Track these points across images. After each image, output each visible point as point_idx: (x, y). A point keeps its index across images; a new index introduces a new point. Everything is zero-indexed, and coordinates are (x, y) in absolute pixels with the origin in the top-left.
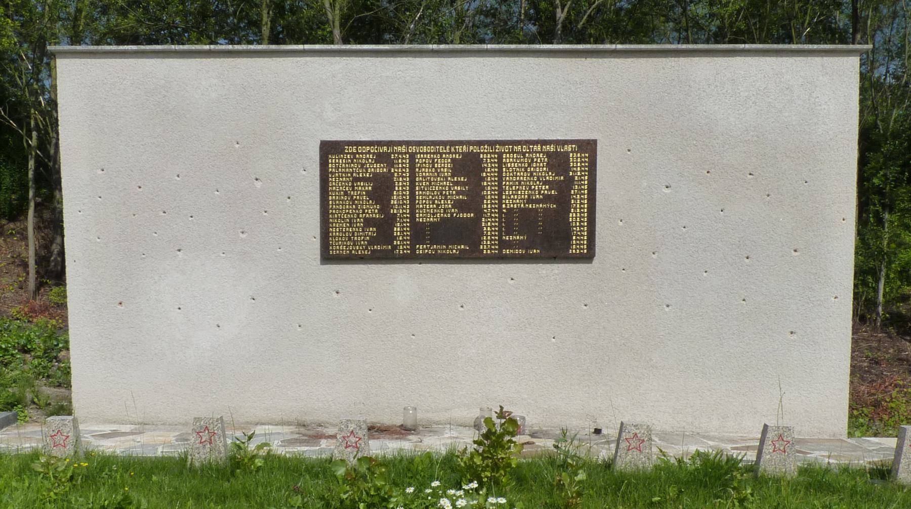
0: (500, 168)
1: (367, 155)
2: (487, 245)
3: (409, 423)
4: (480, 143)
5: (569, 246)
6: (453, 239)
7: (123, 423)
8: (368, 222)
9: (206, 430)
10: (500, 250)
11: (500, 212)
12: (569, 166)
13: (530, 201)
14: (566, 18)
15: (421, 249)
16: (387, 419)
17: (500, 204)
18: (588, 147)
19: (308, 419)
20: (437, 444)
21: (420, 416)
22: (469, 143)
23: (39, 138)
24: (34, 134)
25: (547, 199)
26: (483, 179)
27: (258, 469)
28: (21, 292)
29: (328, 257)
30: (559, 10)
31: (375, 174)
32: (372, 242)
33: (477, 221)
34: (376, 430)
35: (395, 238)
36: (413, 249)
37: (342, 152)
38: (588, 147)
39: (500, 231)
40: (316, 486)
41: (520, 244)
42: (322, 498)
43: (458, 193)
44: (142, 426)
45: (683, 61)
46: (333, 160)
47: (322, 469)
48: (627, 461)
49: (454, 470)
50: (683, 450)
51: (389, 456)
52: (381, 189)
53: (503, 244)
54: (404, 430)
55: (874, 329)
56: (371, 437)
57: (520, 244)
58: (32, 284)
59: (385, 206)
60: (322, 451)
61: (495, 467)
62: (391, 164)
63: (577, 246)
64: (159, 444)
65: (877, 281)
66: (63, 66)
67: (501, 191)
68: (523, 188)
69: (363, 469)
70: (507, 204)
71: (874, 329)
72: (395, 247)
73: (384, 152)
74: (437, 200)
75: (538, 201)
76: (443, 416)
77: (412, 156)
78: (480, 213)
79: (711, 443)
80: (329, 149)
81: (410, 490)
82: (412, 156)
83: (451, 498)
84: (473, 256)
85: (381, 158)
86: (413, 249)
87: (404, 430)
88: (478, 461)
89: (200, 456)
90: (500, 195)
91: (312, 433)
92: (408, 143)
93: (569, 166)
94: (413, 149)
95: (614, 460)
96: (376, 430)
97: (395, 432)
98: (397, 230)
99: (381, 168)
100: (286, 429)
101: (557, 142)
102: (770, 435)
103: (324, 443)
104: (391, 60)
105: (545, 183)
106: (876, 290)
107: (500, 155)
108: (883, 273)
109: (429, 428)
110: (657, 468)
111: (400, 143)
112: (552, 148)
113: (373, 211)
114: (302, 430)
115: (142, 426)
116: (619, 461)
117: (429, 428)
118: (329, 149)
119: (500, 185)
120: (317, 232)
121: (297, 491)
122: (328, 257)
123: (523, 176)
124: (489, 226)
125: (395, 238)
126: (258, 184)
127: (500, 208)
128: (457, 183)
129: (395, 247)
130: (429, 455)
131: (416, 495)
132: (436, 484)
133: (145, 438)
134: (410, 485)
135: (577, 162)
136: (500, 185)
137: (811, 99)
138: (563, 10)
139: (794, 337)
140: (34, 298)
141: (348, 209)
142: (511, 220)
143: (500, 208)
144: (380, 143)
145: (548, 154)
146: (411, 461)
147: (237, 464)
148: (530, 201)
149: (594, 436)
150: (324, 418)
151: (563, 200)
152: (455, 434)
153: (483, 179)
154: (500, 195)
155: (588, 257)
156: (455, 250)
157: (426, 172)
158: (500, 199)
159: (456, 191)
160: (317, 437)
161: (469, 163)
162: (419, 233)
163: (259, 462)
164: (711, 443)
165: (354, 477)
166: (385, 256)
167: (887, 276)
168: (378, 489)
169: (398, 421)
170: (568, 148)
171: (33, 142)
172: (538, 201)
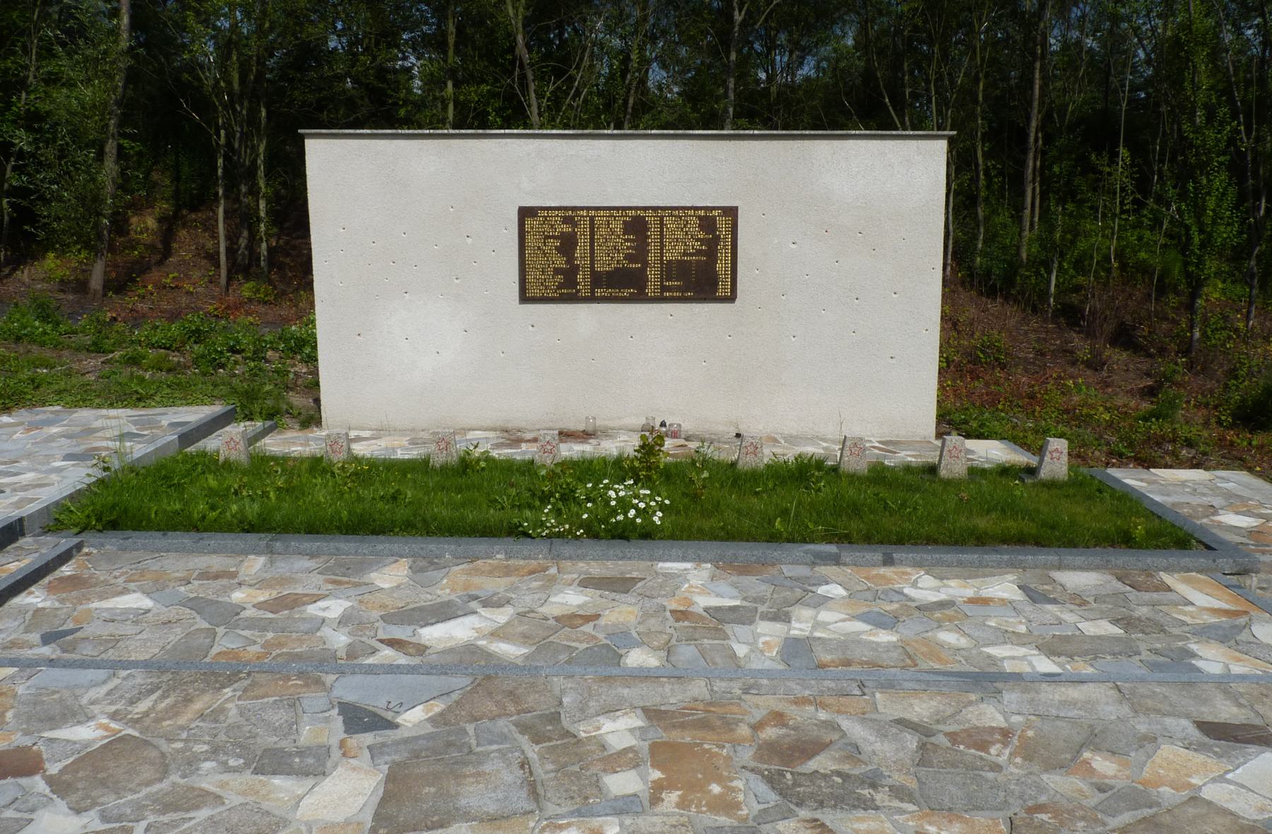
0: (662, 229)
1: (556, 218)
2: (649, 291)
3: (590, 429)
4: (645, 209)
5: (716, 290)
6: (624, 284)
7: (362, 429)
8: (557, 271)
9: (444, 441)
10: (662, 293)
11: (662, 263)
12: (717, 227)
13: (685, 254)
14: (744, 20)
15: (598, 293)
16: (572, 425)
17: (662, 256)
18: (731, 212)
19: (510, 426)
20: (609, 448)
21: (598, 423)
22: (636, 208)
23: (227, 136)
24: (222, 132)
25: (699, 252)
26: (648, 237)
27: (483, 469)
28: (210, 286)
29: (525, 298)
30: (736, 13)
31: (562, 233)
32: (560, 286)
33: (643, 269)
34: (566, 435)
35: (578, 284)
36: (593, 292)
37: (536, 215)
38: (731, 212)
39: (662, 278)
40: (524, 481)
41: (678, 289)
42: (530, 490)
43: (628, 248)
44: (379, 432)
45: (807, 143)
46: (528, 222)
47: (528, 467)
48: (748, 463)
49: (619, 469)
50: (789, 453)
51: (575, 458)
52: (567, 245)
53: (664, 289)
54: (585, 436)
55: (1045, 321)
56: (561, 441)
57: (678, 289)
58: (223, 280)
59: (570, 256)
60: (525, 453)
61: (649, 469)
62: (575, 225)
63: (723, 289)
64: (404, 452)
65: (1050, 273)
66: (309, 144)
67: (662, 246)
68: (678, 245)
69: (558, 470)
70: (668, 256)
71: (1045, 321)
72: (578, 291)
73: (570, 215)
74: (610, 253)
75: (691, 255)
76: (616, 424)
77: (592, 219)
78: (645, 264)
79: (825, 445)
80: (526, 213)
81: (590, 485)
82: (592, 219)
83: (615, 491)
84: (640, 297)
85: (567, 220)
86: (593, 292)
87: (585, 436)
88: (636, 464)
89: (438, 459)
90: (662, 249)
91: (513, 437)
92: (588, 209)
93: (717, 227)
94: (593, 213)
95: (737, 461)
96: (566, 435)
97: (578, 437)
98: (580, 277)
99: (567, 229)
100: (491, 434)
101: (706, 208)
102: (848, 443)
103: (524, 446)
104: (574, 142)
105: (697, 240)
106: (1049, 282)
107: (662, 218)
108: (1056, 265)
109: (606, 433)
110: (768, 466)
111: (582, 208)
112: (702, 213)
113: (561, 262)
114: (506, 435)
115: (379, 432)
116: (740, 463)
117: (606, 433)
118: (526, 213)
119: (661, 242)
120: (516, 278)
121: (512, 485)
122: (525, 298)
123: (680, 235)
124: (652, 274)
125: (578, 284)
126: (469, 241)
127: (662, 260)
128: (627, 240)
129: (578, 291)
130: (604, 459)
131: (594, 488)
132: (606, 481)
133: (383, 443)
134: (590, 481)
135: (722, 225)
136: (661, 242)
137: (899, 182)
138: (740, 12)
139: (893, 361)
140: (227, 294)
141: (542, 261)
142: (669, 270)
143: (662, 260)
144: (566, 209)
145: (700, 217)
146: (591, 462)
147: (466, 465)
148: (685, 254)
149: (735, 440)
150: (523, 424)
151: (711, 254)
152: (626, 438)
153: (648, 237)
154: (662, 249)
155: (731, 298)
156: (625, 293)
157: (603, 231)
158: (662, 253)
159: (626, 245)
160: (517, 442)
161: (637, 223)
162: (598, 279)
163: (483, 464)
164: (825, 445)
165: (552, 476)
166: (571, 297)
167: (1060, 267)
168: (568, 484)
169: (581, 427)
170: (715, 213)
171: (223, 141)
172: (691, 255)
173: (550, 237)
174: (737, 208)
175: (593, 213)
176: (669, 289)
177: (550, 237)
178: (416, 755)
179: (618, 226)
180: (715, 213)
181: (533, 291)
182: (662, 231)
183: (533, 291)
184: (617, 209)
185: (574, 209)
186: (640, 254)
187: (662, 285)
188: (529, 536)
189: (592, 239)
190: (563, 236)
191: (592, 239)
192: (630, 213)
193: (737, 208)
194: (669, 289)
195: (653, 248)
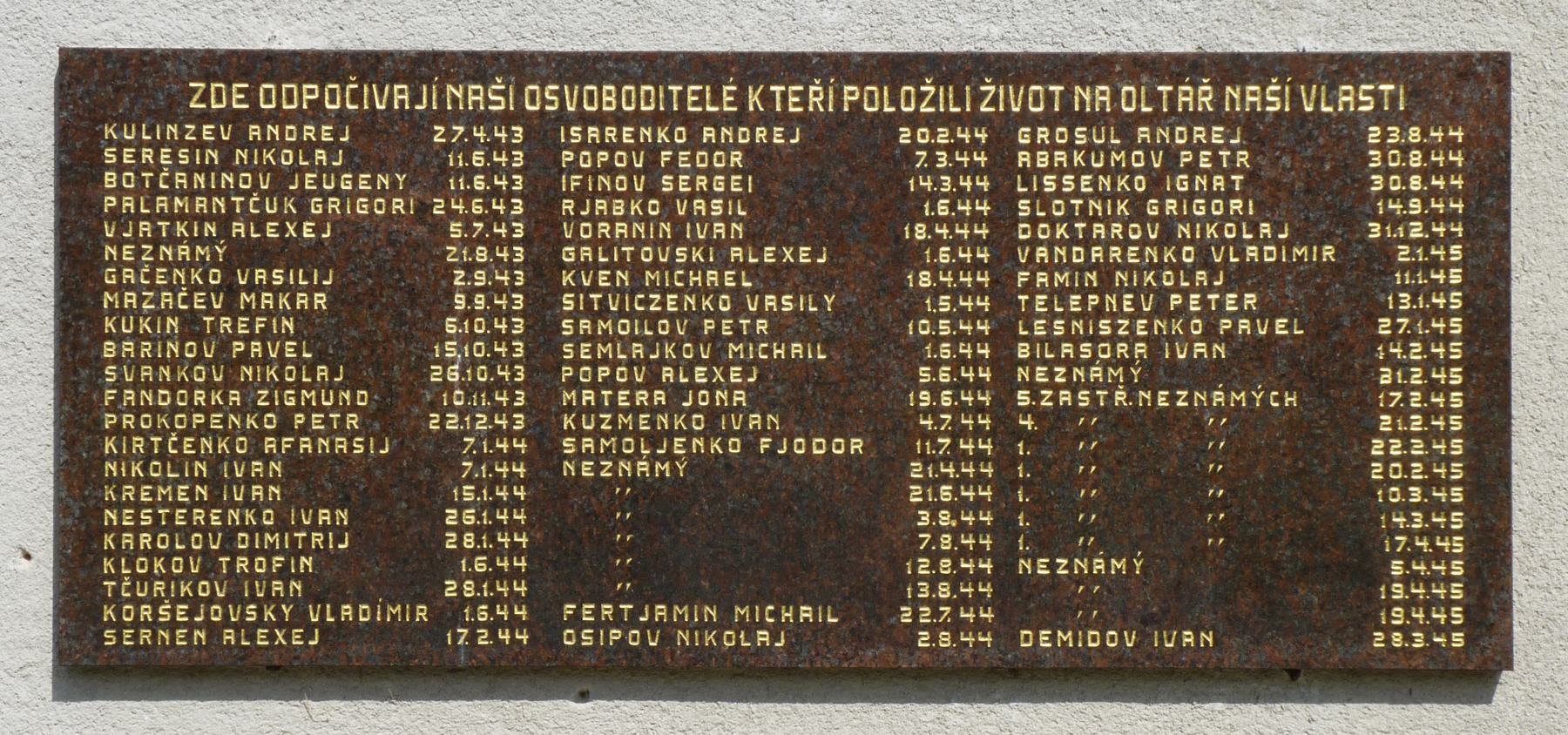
0: (1003, 199)
2: (930, 610)
4: (895, 69)
5: (1368, 615)
8: (308, 479)
10: (1006, 630)
15: (587, 624)
17: (1005, 383)
22: (839, 67)
25: (1249, 359)
31: (348, 227)
33: (880, 478)
35: (449, 563)
36: (546, 623)
37: (173, 110)
38: (1466, 94)
39: (1004, 528)
41: (1113, 604)
43: (781, 329)
46: (124, 149)
52: (380, 304)
53: (1018, 600)
57: (1113, 604)
59: (398, 394)
62: (432, 173)
63: (1416, 603)
68: (1123, 311)
70: (1044, 386)
72: (448, 615)
73: (394, 105)
74: (675, 364)
75: (1200, 375)
77: (544, 134)
78: (896, 435)
80: (103, 94)
85: (372, 142)
86: (546, 623)
90: (1003, 338)
94: (544, 97)
98: (460, 521)
99: (376, 198)
101: (1296, 68)
105: (1240, 277)
107: (1003, 130)
111: (478, 66)
112: (1272, 98)
113: (336, 420)
118: (103, 94)
119: (1002, 290)
123: (1121, 241)
124: (944, 505)
125: (449, 563)
127: (1004, 410)
128: (775, 278)
129: (448, 615)
135: (1405, 169)
136: (1002, 290)
142: (1050, 473)
143: (1004, 410)
145: (1253, 127)
151: (1333, 365)
153: (912, 256)
154: (1003, 338)
156: (764, 629)
157: (618, 218)
158: (1004, 364)
170: (1356, 98)
172: (1200, 375)
173: (263, 253)
174: (1499, 66)
175: (544, 97)
176: (1052, 602)
177: (263, 253)
178: (1498, 294)
179: (713, 182)
180: (1356, 98)
181: (145, 613)
182: (1003, 220)
183: (145, 613)
184: (708, 68)
185: (424, 67)
186: (858, 371)
187: (1005, 575)
188: (574, 668)
189: (544, 273)
190: (347, 249)
191: (544, 273)
192: (786, 96)
193: (1499, 66)
194: (1052, 602)
195: (946, 325)
